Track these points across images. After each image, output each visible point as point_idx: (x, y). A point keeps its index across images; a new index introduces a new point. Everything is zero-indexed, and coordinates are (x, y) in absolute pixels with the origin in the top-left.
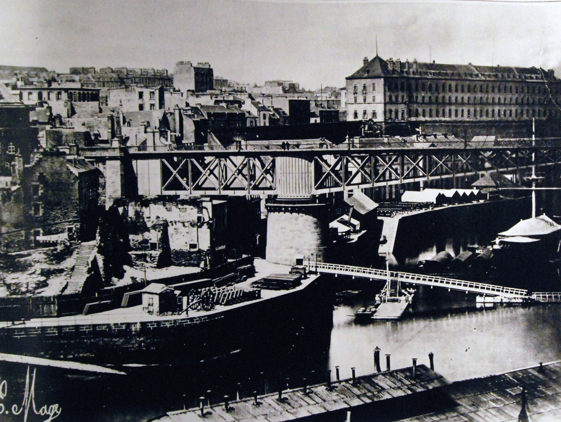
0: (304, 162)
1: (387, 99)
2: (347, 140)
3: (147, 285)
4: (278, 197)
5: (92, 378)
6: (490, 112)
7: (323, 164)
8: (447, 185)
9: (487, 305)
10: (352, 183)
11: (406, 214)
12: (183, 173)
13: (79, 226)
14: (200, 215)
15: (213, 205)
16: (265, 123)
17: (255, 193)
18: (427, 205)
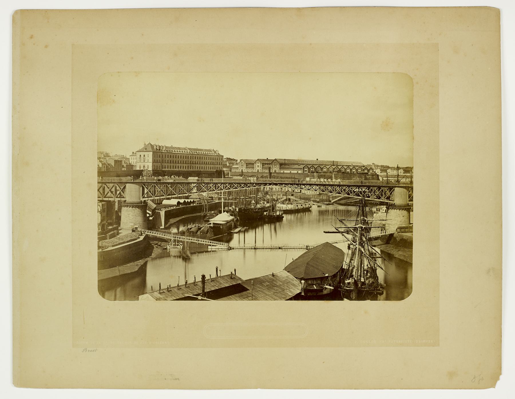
0: (405, 190)
2: (141, 178)
4: (127, 201)
6: (194, 167)
8: (180, 198)
9: (213, 250)
10: (106, 196)
11: (167, 209)
15: (102, 205)
16: (104, 170)
18: (173, 206)
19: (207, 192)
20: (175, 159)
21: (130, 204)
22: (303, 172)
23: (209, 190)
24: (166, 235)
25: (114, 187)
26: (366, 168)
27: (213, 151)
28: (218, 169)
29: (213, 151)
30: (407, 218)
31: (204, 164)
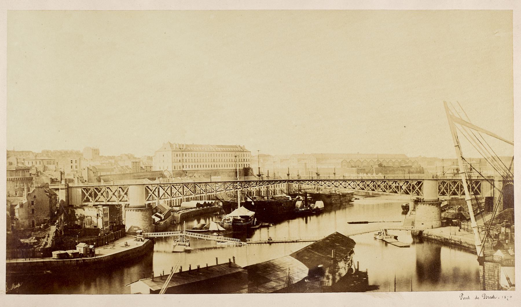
1: (173, 161)
3: (78, 244)
5: (364, 279)
7: (149, 190)
12: (90, 195)
13: (50, 218)
14: (98, 213)
17: (120, 203)
19: (224, 192)
20: (193, 158)
21: (134, 207)
22: (342, 167)
23: (234, 188)
24: (209, 236)
25: (157, 189)
26: (410, 161)
27: (239, 147)
28: (245, 167)
29: (239, 147)
30: (438, 214)
31: (232, 161)
